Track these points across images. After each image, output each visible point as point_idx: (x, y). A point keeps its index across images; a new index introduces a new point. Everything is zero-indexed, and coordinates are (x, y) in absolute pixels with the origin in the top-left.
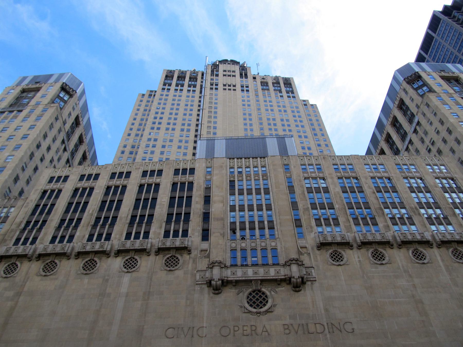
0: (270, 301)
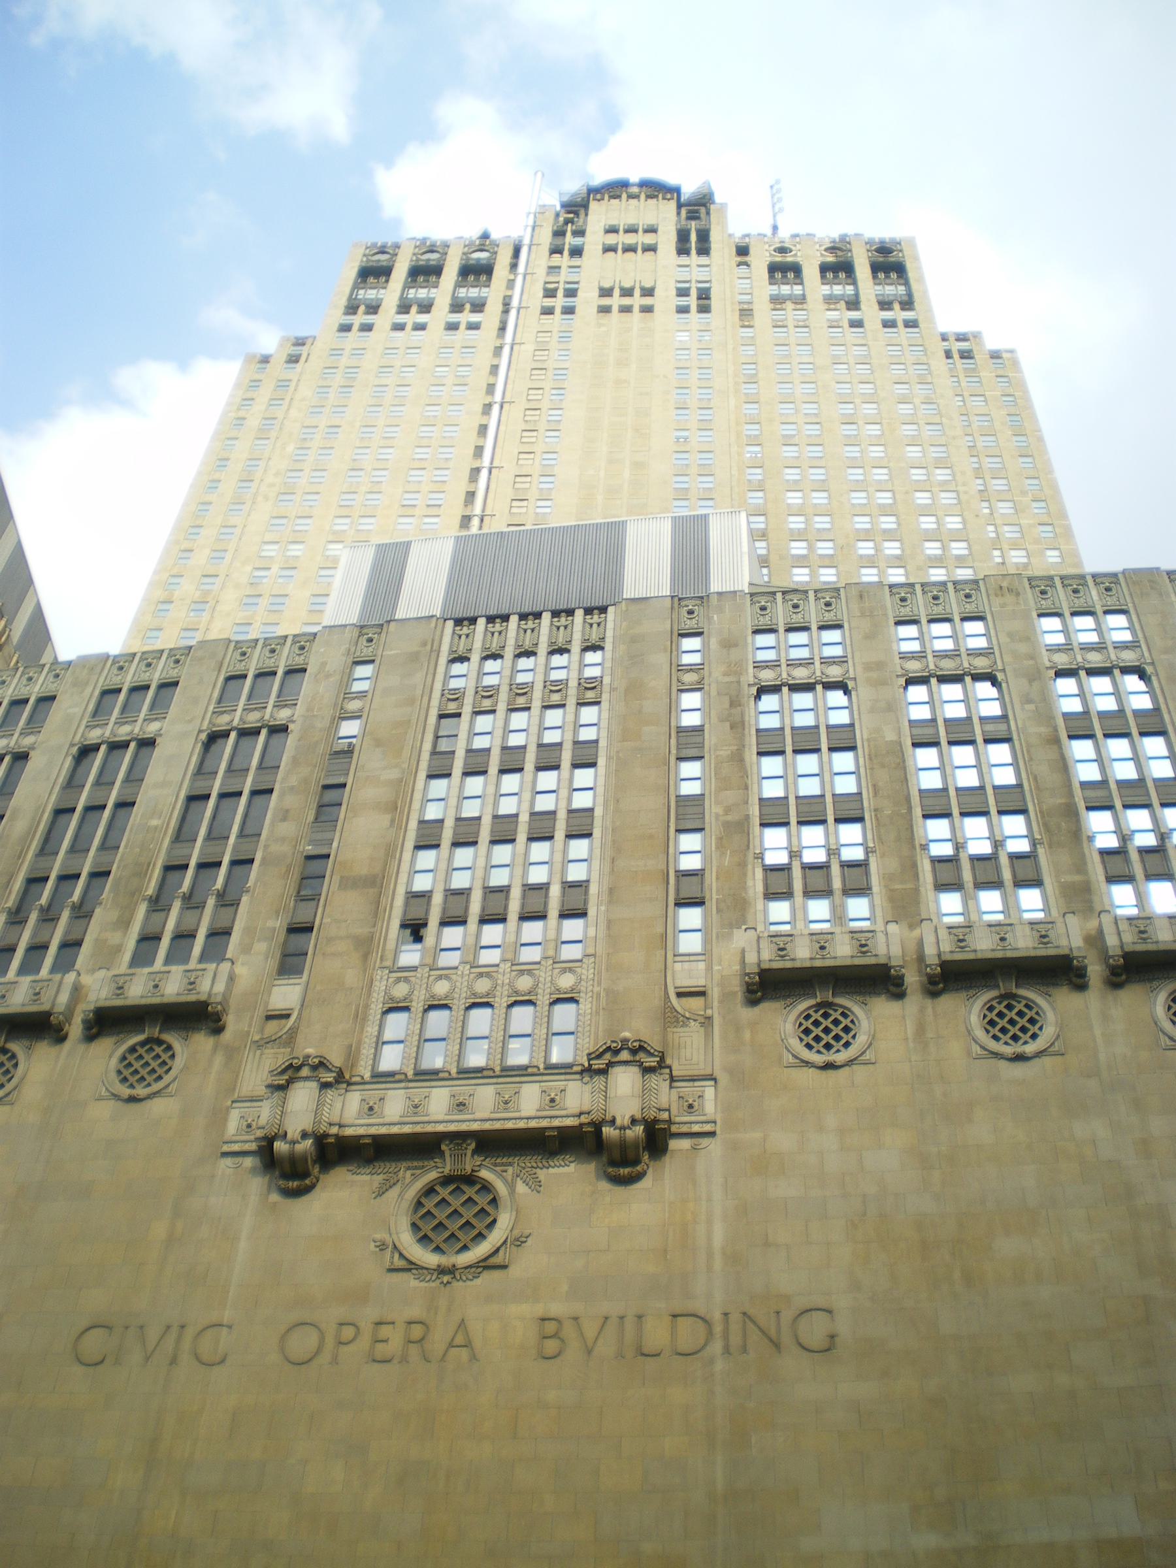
0: (504, 1220)
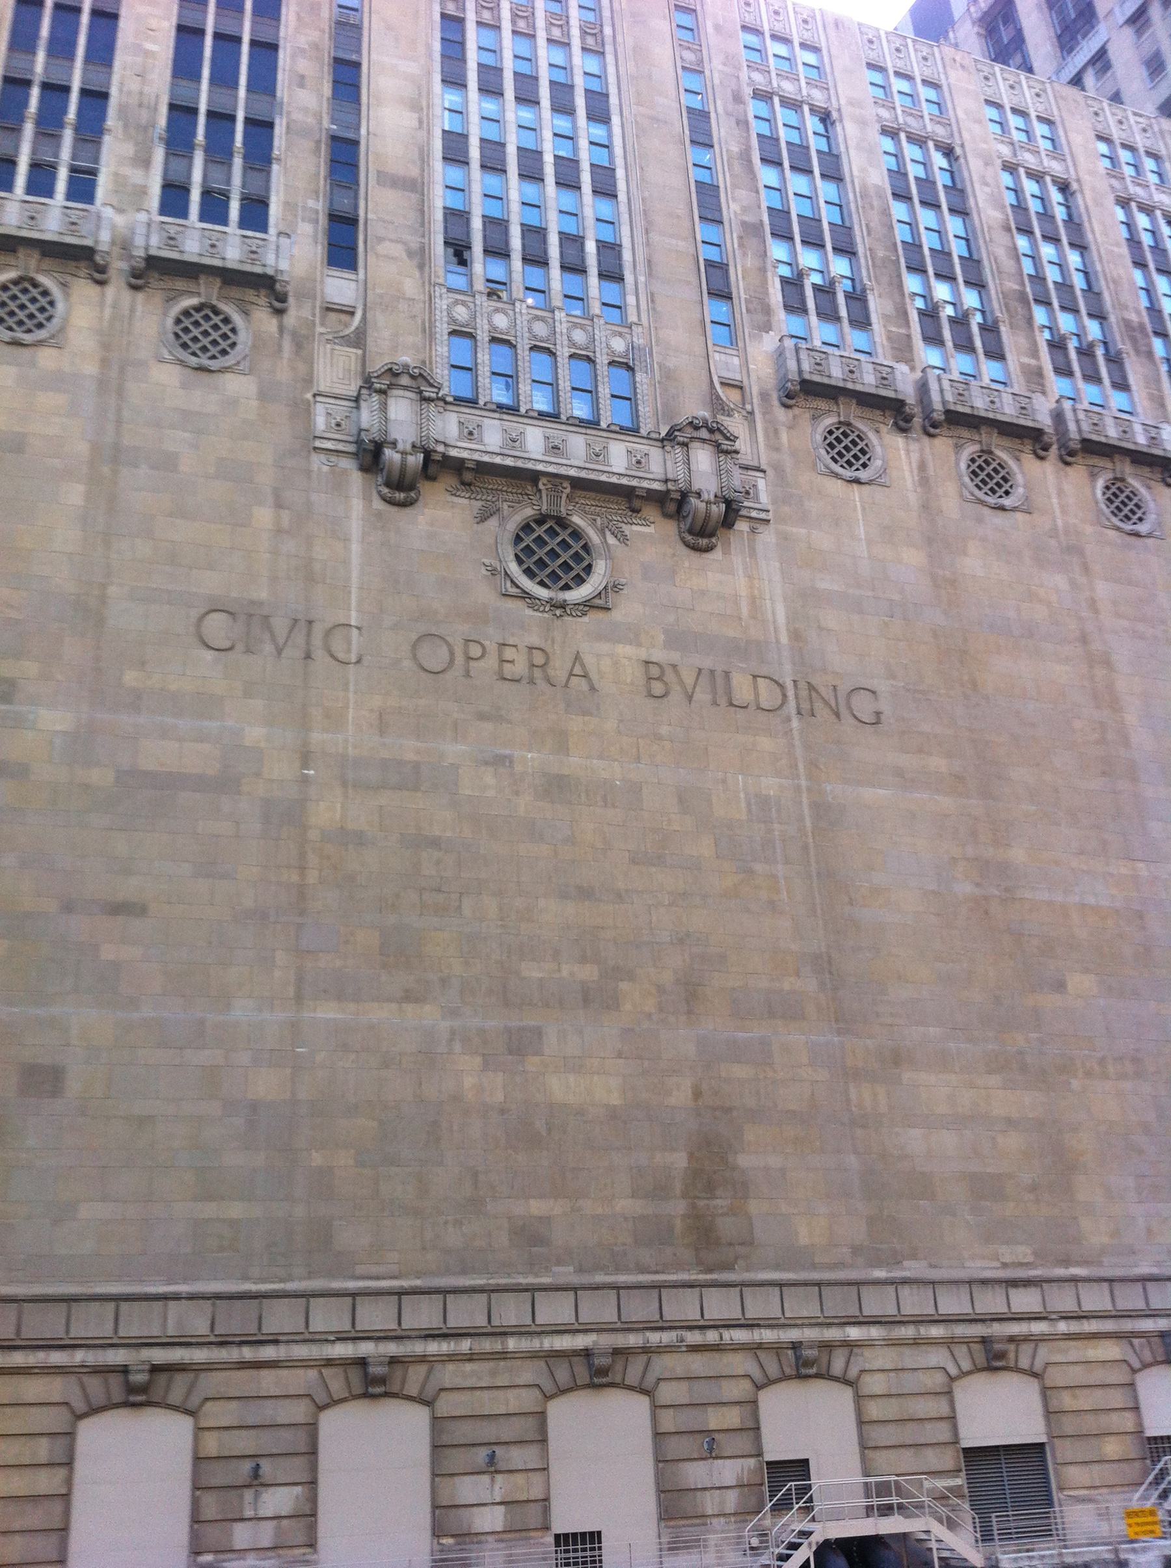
0: (600, 567)
